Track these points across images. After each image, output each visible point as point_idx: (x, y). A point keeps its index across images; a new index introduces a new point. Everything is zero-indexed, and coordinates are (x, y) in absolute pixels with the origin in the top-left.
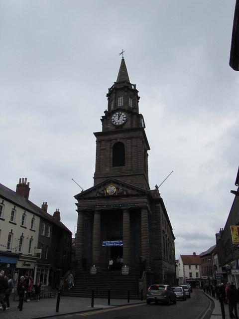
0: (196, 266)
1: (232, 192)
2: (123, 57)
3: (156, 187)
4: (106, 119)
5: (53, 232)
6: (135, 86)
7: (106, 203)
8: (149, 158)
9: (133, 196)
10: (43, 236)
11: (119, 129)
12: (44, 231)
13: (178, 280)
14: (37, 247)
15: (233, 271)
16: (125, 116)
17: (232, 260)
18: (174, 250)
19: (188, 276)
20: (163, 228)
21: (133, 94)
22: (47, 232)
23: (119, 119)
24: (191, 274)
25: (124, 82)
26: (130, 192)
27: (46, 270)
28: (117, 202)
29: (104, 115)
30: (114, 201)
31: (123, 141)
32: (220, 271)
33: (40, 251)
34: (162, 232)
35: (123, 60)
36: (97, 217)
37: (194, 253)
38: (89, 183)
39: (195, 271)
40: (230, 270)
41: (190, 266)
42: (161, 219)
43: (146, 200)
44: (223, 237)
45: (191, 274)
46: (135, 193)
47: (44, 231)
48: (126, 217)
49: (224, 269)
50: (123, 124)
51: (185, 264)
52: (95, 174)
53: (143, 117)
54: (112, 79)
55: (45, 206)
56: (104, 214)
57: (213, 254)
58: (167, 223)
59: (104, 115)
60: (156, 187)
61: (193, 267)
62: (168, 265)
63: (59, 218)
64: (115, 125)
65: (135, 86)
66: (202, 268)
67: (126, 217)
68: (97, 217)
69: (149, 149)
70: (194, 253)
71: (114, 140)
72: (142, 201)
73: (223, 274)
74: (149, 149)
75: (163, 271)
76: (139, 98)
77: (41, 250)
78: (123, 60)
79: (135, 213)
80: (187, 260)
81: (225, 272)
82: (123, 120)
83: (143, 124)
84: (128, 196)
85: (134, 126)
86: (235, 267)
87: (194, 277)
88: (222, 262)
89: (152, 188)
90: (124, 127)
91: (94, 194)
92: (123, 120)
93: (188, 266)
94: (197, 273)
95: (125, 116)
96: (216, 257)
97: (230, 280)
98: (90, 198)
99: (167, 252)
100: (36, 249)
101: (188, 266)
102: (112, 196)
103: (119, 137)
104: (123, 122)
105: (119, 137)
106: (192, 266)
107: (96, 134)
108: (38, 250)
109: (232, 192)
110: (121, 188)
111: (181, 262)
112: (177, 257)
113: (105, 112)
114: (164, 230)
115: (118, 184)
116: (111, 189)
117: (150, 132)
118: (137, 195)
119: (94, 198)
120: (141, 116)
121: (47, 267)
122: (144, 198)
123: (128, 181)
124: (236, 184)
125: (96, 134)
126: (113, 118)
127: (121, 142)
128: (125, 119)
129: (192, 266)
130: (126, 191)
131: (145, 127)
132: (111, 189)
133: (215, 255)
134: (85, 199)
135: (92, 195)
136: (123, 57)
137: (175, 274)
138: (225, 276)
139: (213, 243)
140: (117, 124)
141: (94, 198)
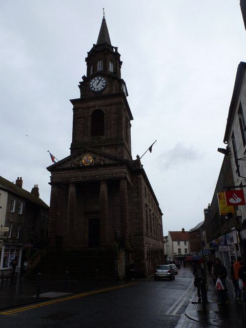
0: (185, 242)
1: (220, 150)
2: (104, 17)
3: (138, 157)
4: (84, 85)
5: (26, 208)
6: (116, 48)
7: (81, 174)
8: (132, 129)
9: (110, 165)
10: (13, 213)
11: (98, 95)
12: (14, 208)
13: (166, 256)
14: (4, 224)
15: (220, 247)
16: (104, 81)
17: (219, 235)
18: (162, 226)
19: (176, 251)
20: (145, 201)
21: (115, 58)
22: (17, 209)
23: (98, 85)
24: (179, 250)
25: (104, 44)
26: (107, 162)
27: (18, 251)
28: (94, 172)
29: (82, 80)
30: (88, 173)
31: (103, 109)
32: (207, 246)
33: (7, 229)
34: (144, 205)
35: (104, 20)
36: (72, 189)
37: (183, 229)
38: (63, 151)
39: (183, 247)
40: (217, 246)
41: (179, 242)
42: (143, 191)
43: (125, 170)
44: (210, 212)
45: (179, 250)
46: (112, 162)
47: (14, 208)
48: (104, 188)
49: (211, 245)
50: (102, 90)
51: (173, 240)
52: (72, 145)
53: (125, 84)
54: (93, 39)
55: (19, 181)
56: (79, 185)
57: (201, 230)
58: (151, 197)
59: (82, 80)
60: (138, 157)
61: (182, 243)
62: (152, 241)
63: (38, 195)
64: (93, 92)
65: (116, 48)
66: (191, 244)
67: (104, 188)
68: (72, 189)
69: (132, 119)
70: (183, 229)
71: (93, 108)
72: (123, 171)
73: (210, 250)
74: (132, 119)
75: (146, 248)
76: (121, 63)
77: (8, 228)
78: (104, 20)
79: (114, 184)
80: (177, 236)
81: (212, 249)
82: (103, 86)
83: (124, 90)
84: (105, 166)
85: (114, 92)
86: (223, 243)
87: (183, 253)
88: (210, 239)
89: (134, 158)
90: (103, 93)
91: (68, 165)
92: (103, 86)
93: (177, 242)
94: (186, 249)
95: (104, 81)
96: (204, 233)
97: (217, 255)
98: (64, 169)
99: (151, 228)
100: (4, 228)
101: (177, 242)
102: (88, 167)
103: (97, 104)
104: (102, 87)
105: (97, 104)
106: (181, 242)
107: (73, 101)
108: (5, 228)
109: (220, 150)
110: (98, 158)
111: (170, 239)
112: (166, 233)
113: (84, 78)
114: (146, 204)
115: (94, 153)
116: (88, 159)
117: (133, 101)
118: (115, 165)
119: (68, 169)
120: (122, 82)
121: (20, 246)
122: (123, 168)
123: (108, 151)
124: (224, 142)
125: (73, 101)
126: (91, 83)
127: (101, 110)
128: (104, 84)
129: (181, 242)
130: (104, 161)
131: (127, 95)
132: (88, 159)
133: (203, 231)
134: (59, 170)
135: (65, 166)
136: (104, 17)
137: (162, 251)
138: (213, 252)
139: (201, 218)
140: (96, 90)
141: (68, 169)
